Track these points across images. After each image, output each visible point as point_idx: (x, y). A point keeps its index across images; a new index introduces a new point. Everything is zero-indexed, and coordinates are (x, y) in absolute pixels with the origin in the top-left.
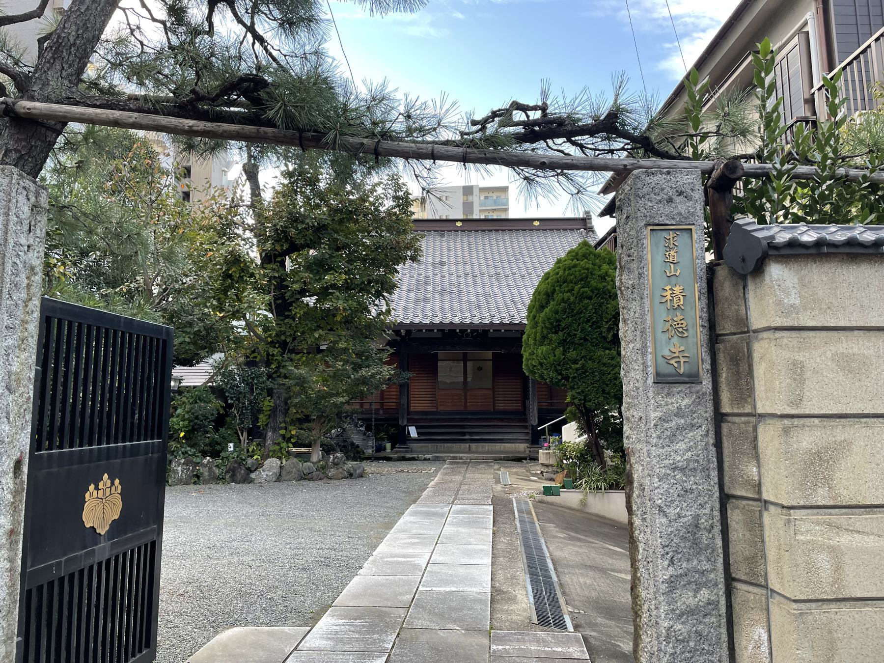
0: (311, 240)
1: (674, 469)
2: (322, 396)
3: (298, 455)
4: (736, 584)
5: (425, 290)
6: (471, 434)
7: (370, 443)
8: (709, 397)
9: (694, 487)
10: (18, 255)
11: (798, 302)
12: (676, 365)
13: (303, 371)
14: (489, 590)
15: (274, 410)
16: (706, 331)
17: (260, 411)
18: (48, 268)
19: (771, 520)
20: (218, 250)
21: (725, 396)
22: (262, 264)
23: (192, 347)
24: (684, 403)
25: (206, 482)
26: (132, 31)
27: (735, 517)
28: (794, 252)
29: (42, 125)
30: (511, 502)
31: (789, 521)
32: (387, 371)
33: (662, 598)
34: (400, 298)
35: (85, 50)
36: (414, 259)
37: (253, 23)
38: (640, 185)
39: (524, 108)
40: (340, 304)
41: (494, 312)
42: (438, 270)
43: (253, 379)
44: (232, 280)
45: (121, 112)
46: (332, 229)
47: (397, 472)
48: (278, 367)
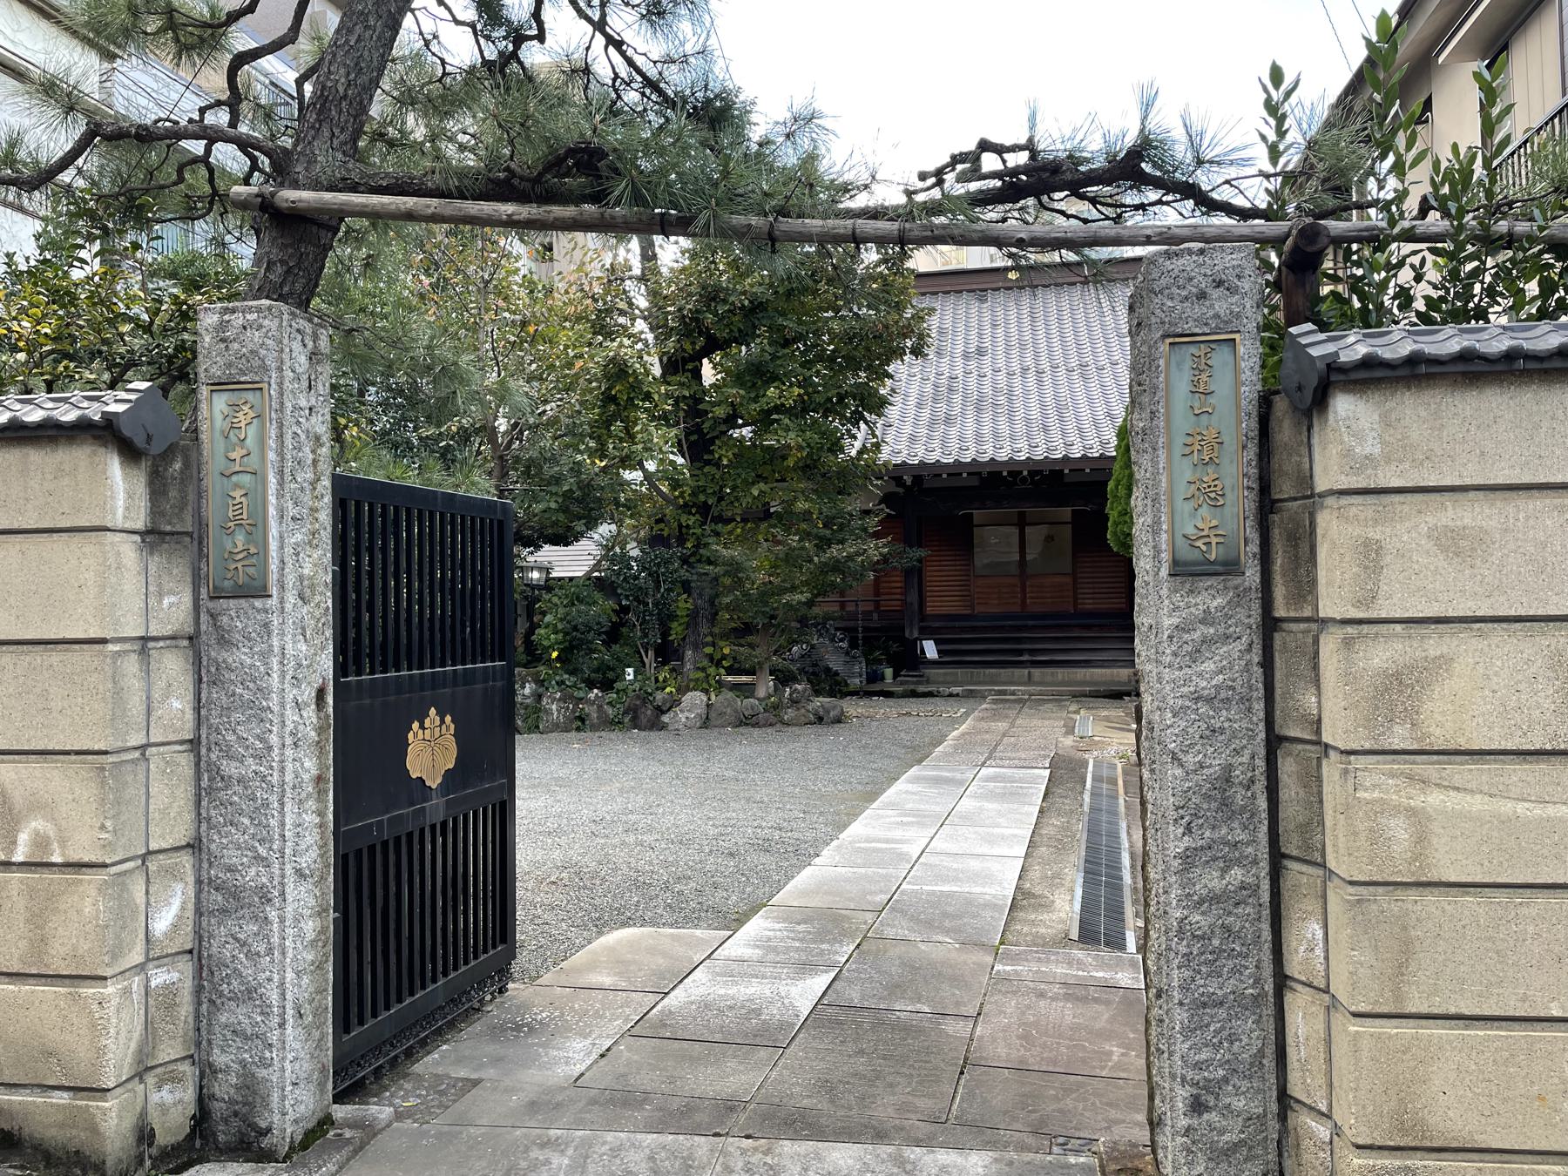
0: (740, 331)
1: (1197, 700)
2: (768, 592)
3: (735, 687)
4: (1286, 862)
5: (949, 401)
6: (1032, 652)
7: (857, 669)
8: (1255, 595)
9: (1226, 725)
10: (298, 423)
11: (1377, 450)
12: (1204, 548)
13: (735, 552)
14: (1010, 893)
15: (694, 615)
16: (1253, 496)
17: (672, 617)
18: (337, 433)
19: (1331, 770)
20: (592, 357)
21: (1279, 592)
22: (663, 375)
23: (561, 517)
24: (1215, 603)
25: (594, 728)
26: (427, 44)
27: (1287, 768)
28: (1372, 375)
29: (313, 221)
30: (1085, 764)
31: (1346, 771)
32: (875, 549)
33: (1174, 878)
34: (903, 419)
35: (361, 102)
36: (917, 352)
37: (603, 15)
38: (1155, 275)
39: (1000, 150)
40: (792, 438)
41: (1073, 437)
42: (972, 365)
43: (658, 565)
44: (618, 404)
45: (415, 199)
46: (776, 310)
47: (900, 715)
48: (697, 546)
